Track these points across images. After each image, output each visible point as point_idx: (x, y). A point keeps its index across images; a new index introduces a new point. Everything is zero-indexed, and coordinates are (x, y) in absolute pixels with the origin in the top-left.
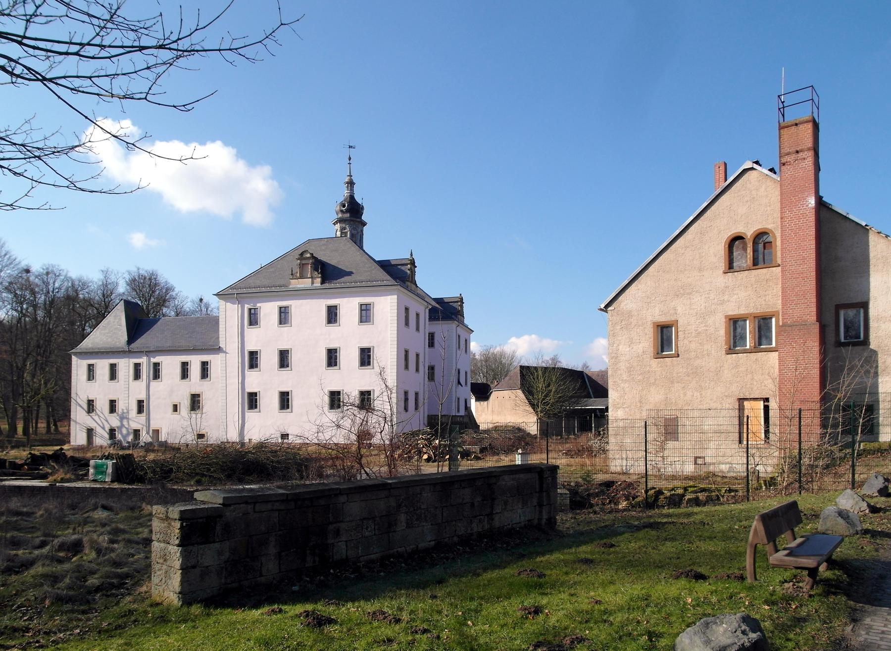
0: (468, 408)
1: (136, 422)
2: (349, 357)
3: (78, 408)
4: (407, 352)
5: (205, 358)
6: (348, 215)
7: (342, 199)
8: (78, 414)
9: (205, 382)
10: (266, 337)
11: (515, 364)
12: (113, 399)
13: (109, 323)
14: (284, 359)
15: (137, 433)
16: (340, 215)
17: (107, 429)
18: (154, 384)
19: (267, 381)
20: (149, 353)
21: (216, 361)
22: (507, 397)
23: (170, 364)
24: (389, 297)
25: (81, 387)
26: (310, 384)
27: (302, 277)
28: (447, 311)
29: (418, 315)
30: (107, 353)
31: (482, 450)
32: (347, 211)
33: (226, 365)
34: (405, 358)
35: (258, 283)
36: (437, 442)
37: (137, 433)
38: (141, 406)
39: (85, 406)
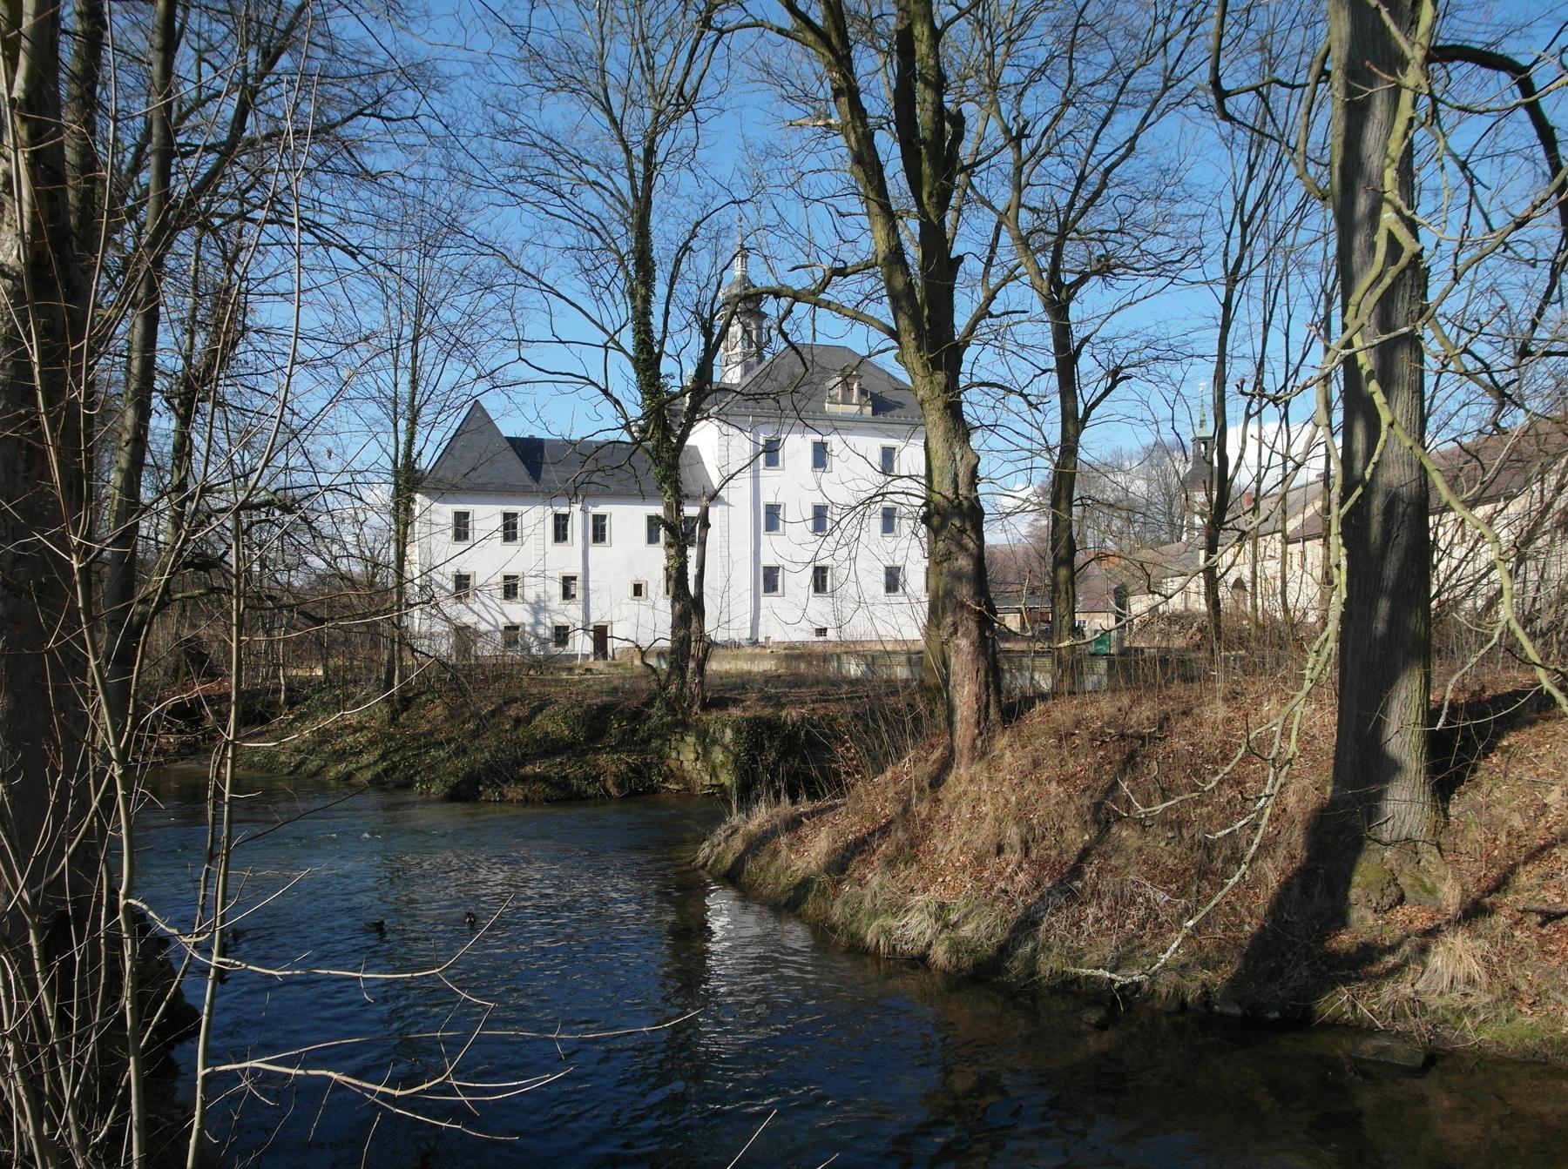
18: (595, 550)
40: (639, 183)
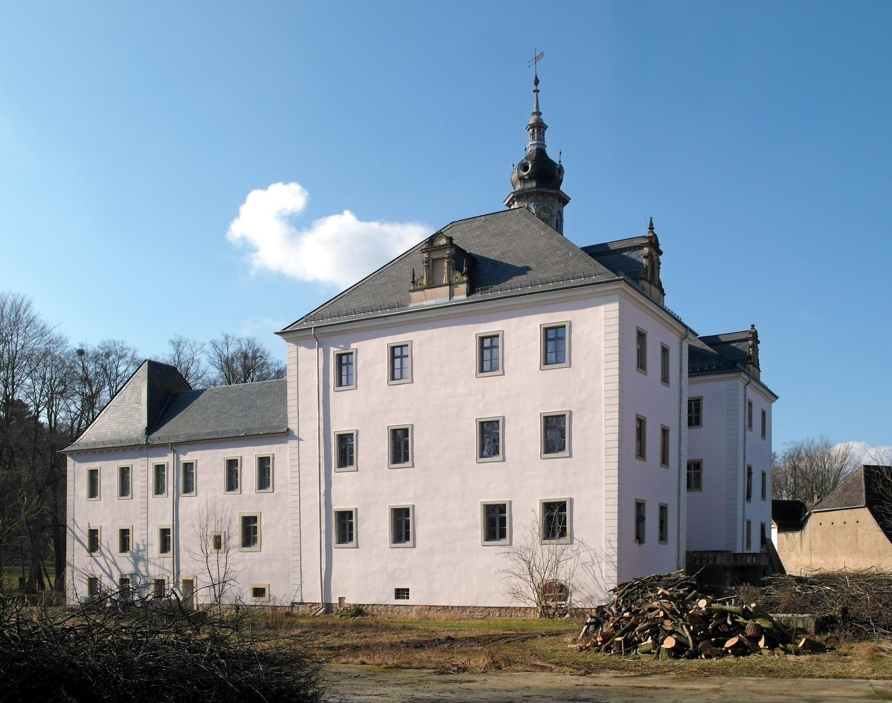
0: (765, 541)
1: (158, 566)
2: (523, 436)
3: (76, 543)
4: (641, 423)
5: (264, 450)
6: (534, 184)
7: (521, 157)
8: (77, 554)
9: (265, 495)
10: (368, 407)
11: (849, 469)
12: (121, 527)
13: (123, 400)
14: (400, 446)
15: (160, 583)
16: (519, 187)
17: (117, 578)
18: (185, 500)
19: (371, 490)
20: (177, 446)
21: (281, 454)
22: (838, 523)
23: (209, 464)
24: (602, 308)
25: (83, 512)
26: (449, 488)
27: (432, 285)
28: (727, 358)
29: (665, 351)
30: (109, 450)
31: (823, 625)
32: (531, 178)
33: (299, 461)
34: (637, 436)
35: (354, 305)
36: (702, 603)
37: (160, 583)
38: (166, 539)
39: (86, 541)
40: (632, 674)
